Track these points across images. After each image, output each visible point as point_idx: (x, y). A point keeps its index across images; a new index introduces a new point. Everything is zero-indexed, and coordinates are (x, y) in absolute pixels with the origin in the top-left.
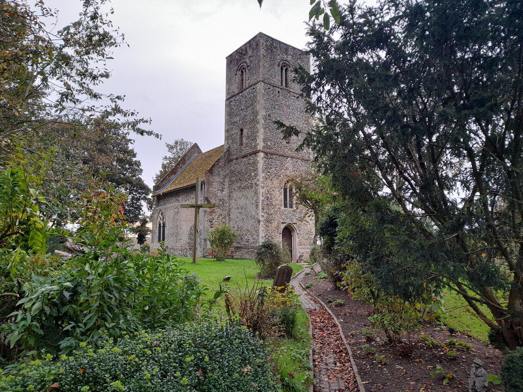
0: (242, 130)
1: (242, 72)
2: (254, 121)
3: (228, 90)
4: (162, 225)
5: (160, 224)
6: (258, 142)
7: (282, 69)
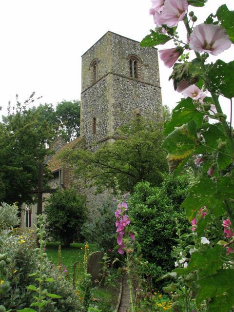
0: (95, 119)
1: (95, 67)
2: (105, 109)
3: (83, 84)
4: (29, 212)
5: (27, 211)
6: (108, 129)
7: (131, 62)
